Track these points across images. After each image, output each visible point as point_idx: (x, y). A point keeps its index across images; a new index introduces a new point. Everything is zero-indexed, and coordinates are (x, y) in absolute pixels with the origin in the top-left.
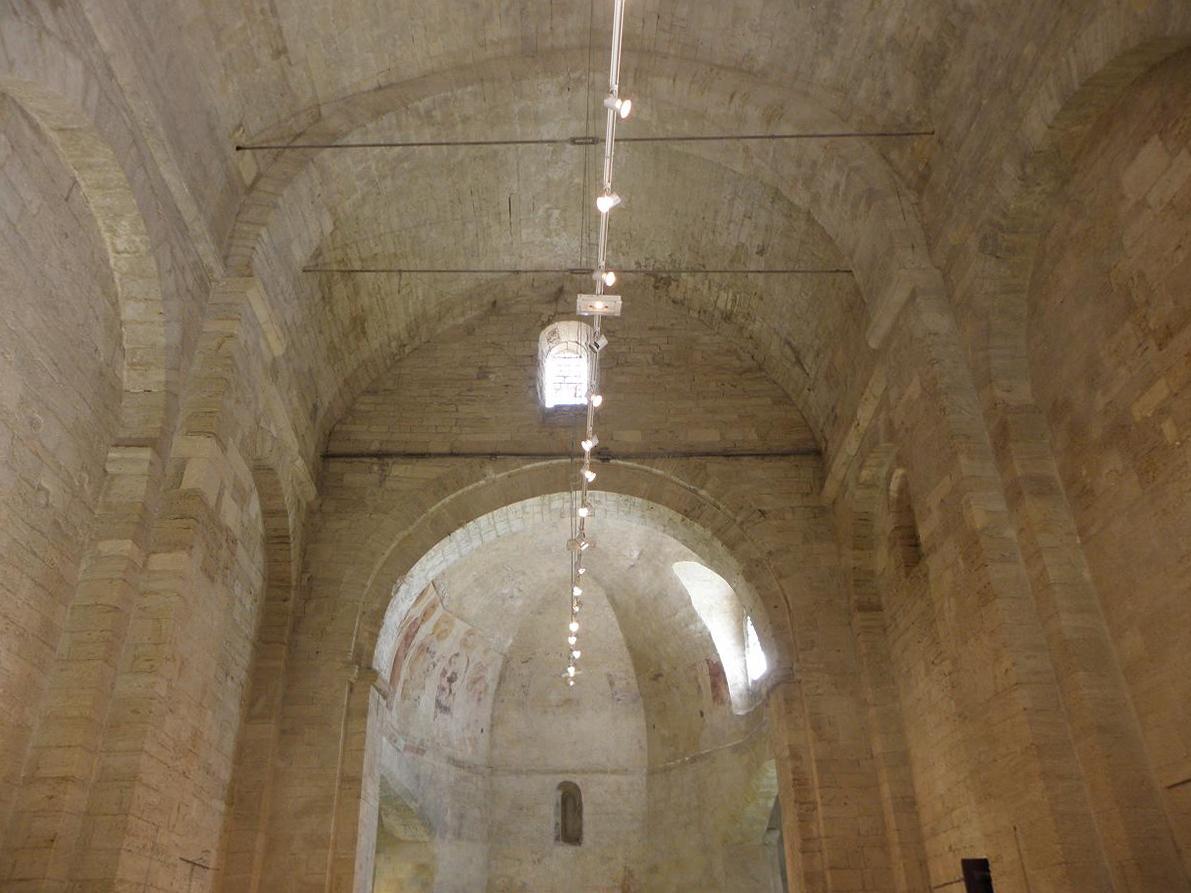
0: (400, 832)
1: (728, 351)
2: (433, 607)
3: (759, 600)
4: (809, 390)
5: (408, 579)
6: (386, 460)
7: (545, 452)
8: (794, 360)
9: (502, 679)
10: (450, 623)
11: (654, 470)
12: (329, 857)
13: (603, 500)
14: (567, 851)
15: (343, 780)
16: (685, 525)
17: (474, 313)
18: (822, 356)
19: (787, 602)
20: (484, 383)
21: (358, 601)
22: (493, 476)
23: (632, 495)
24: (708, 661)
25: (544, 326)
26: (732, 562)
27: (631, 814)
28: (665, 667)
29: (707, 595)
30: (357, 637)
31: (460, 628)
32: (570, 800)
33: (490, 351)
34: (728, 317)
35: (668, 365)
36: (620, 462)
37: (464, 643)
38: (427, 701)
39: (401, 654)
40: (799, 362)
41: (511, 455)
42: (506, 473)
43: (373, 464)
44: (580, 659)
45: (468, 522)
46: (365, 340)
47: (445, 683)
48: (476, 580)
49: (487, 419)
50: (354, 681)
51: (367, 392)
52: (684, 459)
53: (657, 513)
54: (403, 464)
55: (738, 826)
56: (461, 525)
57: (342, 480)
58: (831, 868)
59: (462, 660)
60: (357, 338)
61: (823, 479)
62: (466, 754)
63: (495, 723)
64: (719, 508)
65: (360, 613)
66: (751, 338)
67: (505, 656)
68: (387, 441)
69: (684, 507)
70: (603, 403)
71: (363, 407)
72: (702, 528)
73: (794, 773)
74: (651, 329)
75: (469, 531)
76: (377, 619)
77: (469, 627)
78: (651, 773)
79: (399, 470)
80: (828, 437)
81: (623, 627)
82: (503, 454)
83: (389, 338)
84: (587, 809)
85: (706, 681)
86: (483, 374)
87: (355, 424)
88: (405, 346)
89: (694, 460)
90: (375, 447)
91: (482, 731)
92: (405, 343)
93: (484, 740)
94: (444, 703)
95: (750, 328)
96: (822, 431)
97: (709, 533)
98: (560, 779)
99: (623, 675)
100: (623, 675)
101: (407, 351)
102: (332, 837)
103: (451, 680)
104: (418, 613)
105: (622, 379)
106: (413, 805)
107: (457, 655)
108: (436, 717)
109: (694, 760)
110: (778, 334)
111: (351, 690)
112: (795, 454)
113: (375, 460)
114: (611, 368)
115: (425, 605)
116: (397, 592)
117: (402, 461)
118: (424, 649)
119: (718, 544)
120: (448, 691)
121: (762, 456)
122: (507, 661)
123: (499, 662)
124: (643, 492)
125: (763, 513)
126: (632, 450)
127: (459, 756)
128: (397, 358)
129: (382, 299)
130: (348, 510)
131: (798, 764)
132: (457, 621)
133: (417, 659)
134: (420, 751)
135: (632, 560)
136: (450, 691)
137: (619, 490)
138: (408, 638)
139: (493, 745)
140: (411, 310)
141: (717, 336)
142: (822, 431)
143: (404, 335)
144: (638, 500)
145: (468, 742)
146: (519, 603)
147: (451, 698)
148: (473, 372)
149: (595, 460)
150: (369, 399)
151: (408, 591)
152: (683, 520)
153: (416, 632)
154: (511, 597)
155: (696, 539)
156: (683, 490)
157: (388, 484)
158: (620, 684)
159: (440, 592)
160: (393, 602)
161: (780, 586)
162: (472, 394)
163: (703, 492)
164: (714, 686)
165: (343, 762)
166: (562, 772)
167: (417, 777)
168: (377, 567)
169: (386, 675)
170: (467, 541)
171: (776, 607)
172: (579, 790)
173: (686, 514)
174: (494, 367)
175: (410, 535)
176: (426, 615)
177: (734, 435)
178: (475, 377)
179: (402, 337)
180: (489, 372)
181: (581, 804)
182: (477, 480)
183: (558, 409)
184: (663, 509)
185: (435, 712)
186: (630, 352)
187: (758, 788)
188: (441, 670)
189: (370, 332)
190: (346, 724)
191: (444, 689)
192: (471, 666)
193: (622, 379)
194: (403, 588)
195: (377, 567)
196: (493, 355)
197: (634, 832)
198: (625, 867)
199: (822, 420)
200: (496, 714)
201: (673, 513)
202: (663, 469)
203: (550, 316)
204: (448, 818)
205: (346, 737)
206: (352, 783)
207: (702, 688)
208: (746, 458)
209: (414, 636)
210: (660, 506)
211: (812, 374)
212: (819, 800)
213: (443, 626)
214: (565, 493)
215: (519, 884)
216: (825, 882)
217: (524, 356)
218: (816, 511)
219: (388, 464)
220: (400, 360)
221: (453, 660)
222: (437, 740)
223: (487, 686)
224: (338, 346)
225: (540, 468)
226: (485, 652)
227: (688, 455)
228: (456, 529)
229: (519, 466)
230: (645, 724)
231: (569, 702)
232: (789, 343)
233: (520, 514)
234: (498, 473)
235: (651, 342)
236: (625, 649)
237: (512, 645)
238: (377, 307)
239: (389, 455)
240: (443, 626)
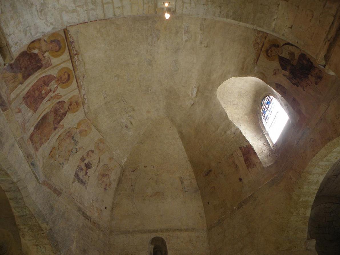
24: (240, 148)
31: (94, 135)
44: (168, 20)
47: (83, 165)
63: (114, 206)
77: (101, 137)
78: (210, 228)
81: (187, 150)
98: (153, 235)
106: (44, 226)
109: (240, 206)
120: (84, 172)
122: (123, 171)
132: (93, 128)
146: (130, 133)
147: (86, 177)
164: (247, 160)
192: (101, 164)
213: (83, 127)
236: (189, 162)
237: (126, 162)
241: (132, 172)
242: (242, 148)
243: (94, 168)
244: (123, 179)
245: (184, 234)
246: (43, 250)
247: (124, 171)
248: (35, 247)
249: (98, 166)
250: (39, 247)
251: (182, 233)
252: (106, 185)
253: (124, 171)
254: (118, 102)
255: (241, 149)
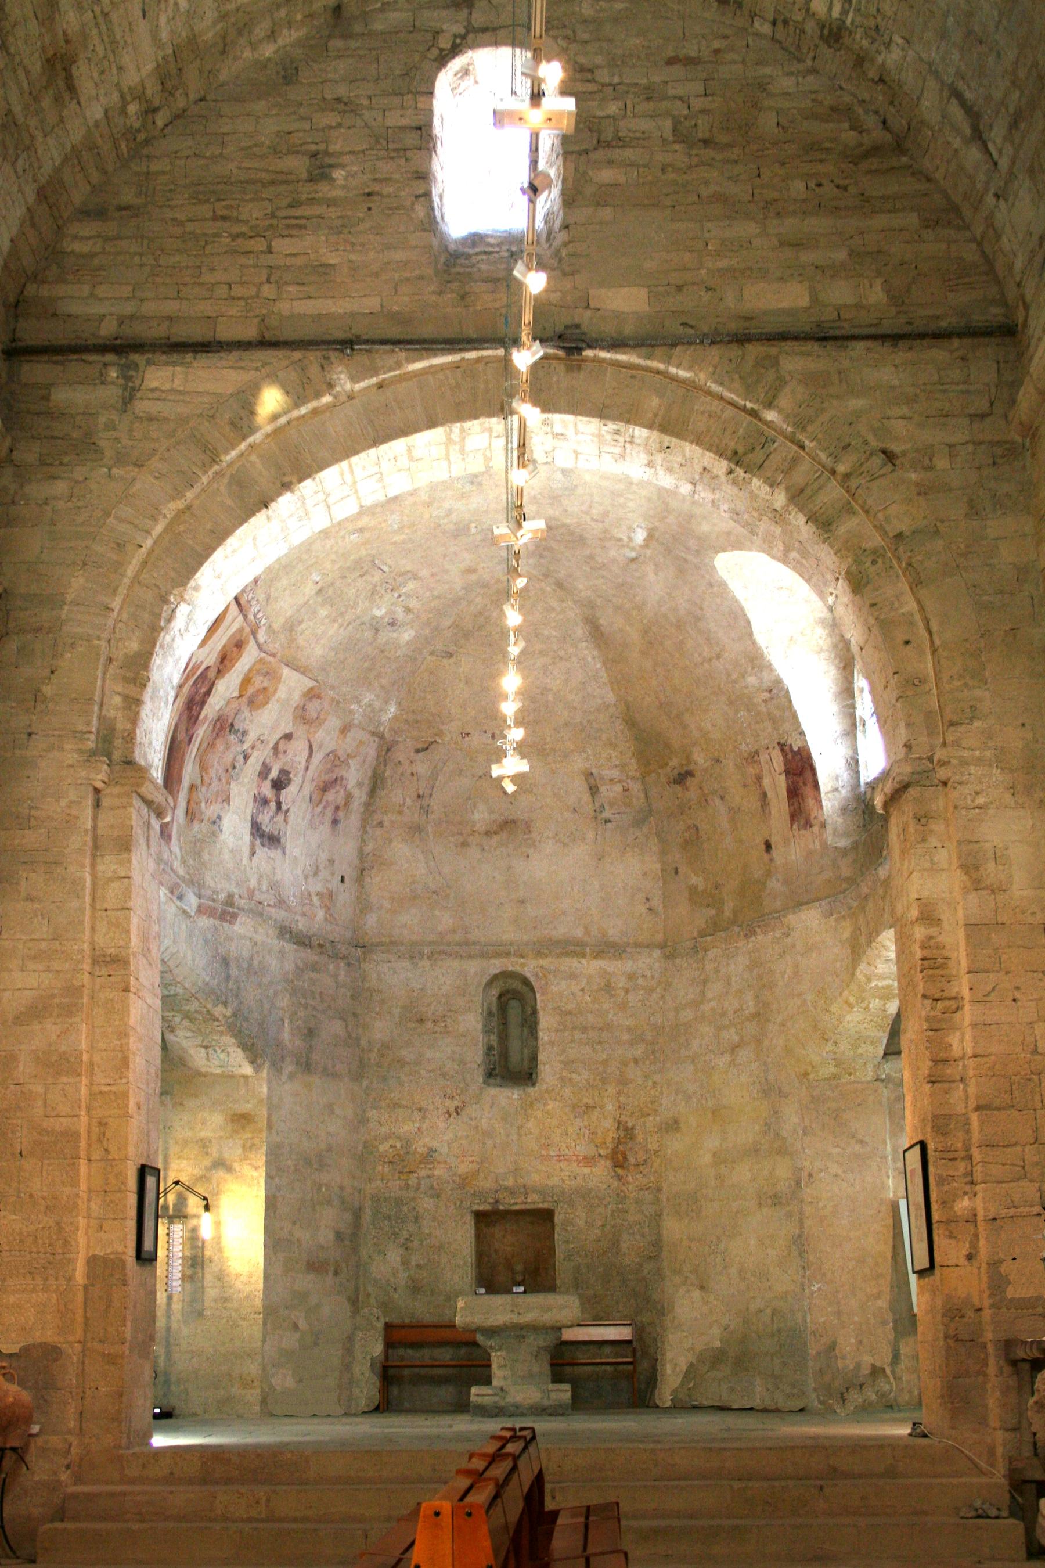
0: (198, 1058)
1: (833, 109)
2: (239, 645)
3: (875, 630)
4: (997, 196)
5: (189, 593)
6: (135, 357)
7: (443, 331)
8: (968, 131)
9: (376, 783)
10: (271, 674)
11: (673, 370)
12: (83, 1091)
13: (570, 432)
14: (509, 1096)
15: (95, 962)
16: (735, 482)
17: (296, 34)
18: (1022, 125)
19: (930, 633)
20: (324, 189)
21: (99, 638)
22: (348, 386)
23: (628, 422)
24: (782, 746)
25: (442, 60)
26: (827, 555)
27: (629, 1029)
28: (700, 759)
29: (787, 617)
30: (101, 705)
32: (512, 1005)
33: (330, 118)
34: (834, 34)
35: (706, 142)
36: (604, 355)
37: (301, 715)
38: (234, 826)
39: (181, 736)
40: (978, 136)
41: (384, 342)
42: (374, 380)
43: (105, 365)
44: (531, 767)
45: (301, 480)
46: (73, 105)
47: (267, 791)
48: (320, 591)
49: (333, 266)
50: (99, 785)
51: (86, 213)
52: (734, 346)
53: (679, 459)
54: (166, 364)
55: (830, 1047)
56: (287, 487)
57: (46, 398)
58: (978, 1108)
59: (297, 750)
60: (58, 100)
61: (1015, 385)
62: (315, 921)
64: (802, 447)
65: (103, 659)
66: (882, 80)
67: (382, 737)
68: (132, 317)
69: (732, 445)
70: (548, 282)
71: (78, 247)
72: (768, 489)
73: (923, 947)
74: (671, 61)
75: (303, 499)
76: (137, 670)
79: (160, 376)
80: (1028, 298)
82: (367, 342)
83: (122, 97)
84: (546, 1022)
85: (777, 784)
86: (321, 170)
87: (64, 281)
88: (156, 110)
89: (754, 350)
90: (107, 330)
91: (342, 880)
92: (157, 103)
93: (345, 897)
94: (267, 828)
95: (880, 59)
96: (1019, 285)
97: (780, 499)
98: (496, 966)
99: (615, 773)
100: (615, 773)
101: (160, 123)
102: (85, 1057)
103: (278, 785)
104: (210, 658)
105: (607, 175)
107: (288, 737)
108: (253, 854)
110: (936, 74)
111: (97, 804)
112: (960, 335)
113: (110, 357)
114: (586, 151)
115: (224, 641)
116: (170, 620)
117: (164, 357)
118: (224, 726)
119: (799, 520)
120: (273, 805)
121: (894, 338)
122: (386, 748)
123: (371, 752)
124: (650, 415)
125: (889, 456)
126: (628, 330)
127: (301, 925)
128: (141, 137)
129: (106, 15)
130: (66, 460)
131: (933, 931)
132: (286, 671)
133: (211, 745)
134: (226, 911)
135: (633, 549)
136: (279, 805)
137: (601, 412)
138: (192, 705)
139: (363, 906)
140: (164, 35)
141: (811, 78)
142: (1019, 285)
143: (152, 89)
144: (640, 433)
145: (315, 899)
146: (407, 635)
147: (280, 818)
148: (299, 165)
149: (551, 351)
150: (87, 229)
151: (190, 617)
152: (731, 472)
153: (208, 693)
154: (392, 624)
155: (757, 510)
156: (730, 412)
157: (141, 406)
158: (609, 792)
159: (251, 617)
160: (165, 638)
161: (919, 602)
162: (298, 212)
163: (771, 416)
164: (793, 793)
165: (93, 929)
166: (498, 955)
167: (225, 962)
168: (130, 571)
169: (157, 774)
170: (300, 519)
171: (907, 642)
172: (532, 990)
173: (736, 458)
174: (341, 154)
175: (189, 508)
176: (225, 661)
177: (840, 293)
178: (304, 176)
179: (149, 92)
180: (331, 166)
181: (535, 1012)
182: (318, 395)
183: (475, 239)
184: (690, 449)
185: (253, 846)
186: (625, 116)
187: (869, 980)
188: (258, 768)
189: (86, 86)
190: (93, 865)
191: (265, 802)
192: (318, 757)
193: (607, 175)
194: (183, 610)
195: (130, 571)
196: (340, 125)
197: (636, 1061)
198: (619, 1123)
199: (1019, 264)
200: (369, 848)
201: (708, 458)
202: (690, 368)
203: (455, 36)
204: (286, 1035)
205: (94, 884)
206: (113, 963)
207: (770, 795)
208: (861, 345)
209: (203, 703)
210: (683, 443)
211: (1004, 163)
212: (966, 992)
213: (259, 682)
214: (494, 420)
215: (422, 1150)
216: (968, 1132)
217: (403, 128)
218: (999, 451)
219: (136, 367)
220: (147, 142)
221: (281, 746)
222: (258, 896)
223: (349, 796)
224: (21, 120)
225: (442, 367)
226: (344, 730)
227: (741, 339)
228: (280, 494)
229: (399, 365)
230: (658, 866)
231: (510, 827)
232: (958, 95)
233: (404, 462)
234: (358, 382)
235: (671, 92)
237: (395, 718)
238: (95, 32)
239: (138, 346)
240: (259, 682)
241: (418, 751)
242: (787, 748)
243: (296, 781)
244: (388, 773)
245: (591, 967)
246: (222, 1056)
247: (388, 750)
248: (203, 1050)
249: (307, 768)
250: (211, 1051)
251: (584, 961)
252: (337, 808)
253: (388, 750)
254: (361, 576)
255: (782, 750)
